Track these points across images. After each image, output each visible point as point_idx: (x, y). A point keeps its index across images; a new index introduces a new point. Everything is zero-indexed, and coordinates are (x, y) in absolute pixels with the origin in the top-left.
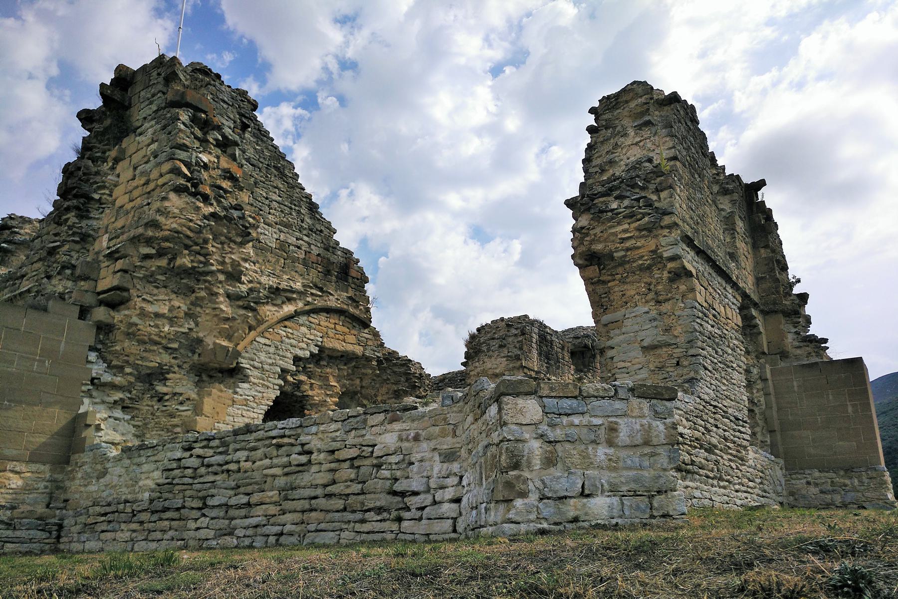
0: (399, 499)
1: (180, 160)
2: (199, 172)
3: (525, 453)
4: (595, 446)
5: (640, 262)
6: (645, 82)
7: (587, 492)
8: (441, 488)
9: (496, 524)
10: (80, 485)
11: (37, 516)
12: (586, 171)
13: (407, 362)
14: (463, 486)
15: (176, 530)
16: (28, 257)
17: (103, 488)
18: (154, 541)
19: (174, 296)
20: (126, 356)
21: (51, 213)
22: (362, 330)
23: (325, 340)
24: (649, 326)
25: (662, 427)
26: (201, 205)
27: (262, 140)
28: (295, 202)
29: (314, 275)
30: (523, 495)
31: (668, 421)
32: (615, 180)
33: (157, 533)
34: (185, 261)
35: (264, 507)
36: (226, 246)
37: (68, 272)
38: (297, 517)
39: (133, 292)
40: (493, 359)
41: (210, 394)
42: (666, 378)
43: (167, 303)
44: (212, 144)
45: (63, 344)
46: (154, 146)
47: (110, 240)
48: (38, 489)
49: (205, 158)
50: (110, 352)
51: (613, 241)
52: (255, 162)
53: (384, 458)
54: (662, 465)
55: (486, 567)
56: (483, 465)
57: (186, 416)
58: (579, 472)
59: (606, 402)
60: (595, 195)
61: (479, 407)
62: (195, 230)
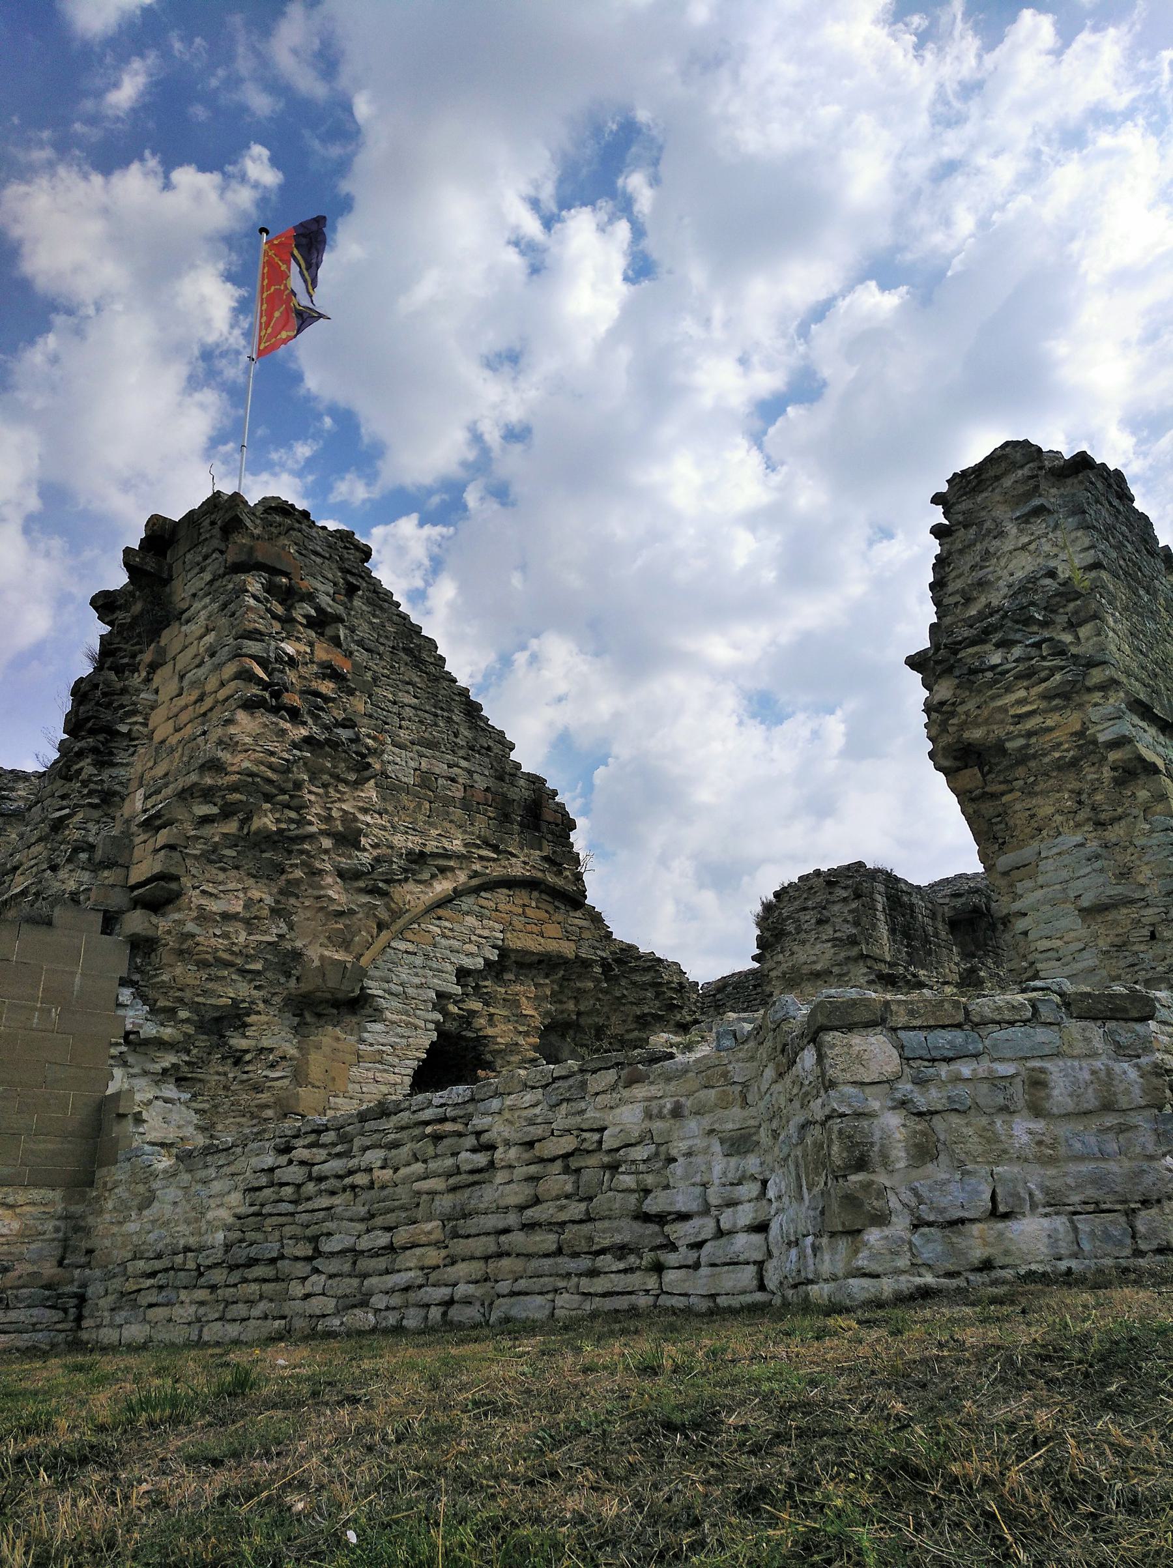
0: (653, 1228)
1: (251, 657)
2: (282, 671)
3: (876, 1138)
4: (1007, 1118)
5: (1057, 755)
6: (1026, 441)
7: (1002, 1208)
8: (728, 1205)
9: (834, 1278)
10: (112, 1223)
11: (44, 1282)
12: (937, 602)
13: (655, 963)
14: (770, 1200)
15: (271, 1300)
16: (21, 836)
17: (149, 1226)
18: (235, 1320)
19: (252, 881)
20: (179, 989)
21: (56, 762)
22: (571, 914)
23: (509, 935)
24: (1089, 869)
25: (1133, 1074)
26: (288, 726)
27: (382, 609)
28: (441, 704)
29: (481, 825)
30: (881, 1219)
31: (1143, 1060)
32: (991, 615)
33: (240, 1305)
34: (267, 821)
35: (418, 1251)
36: (331, 790)
37: (83, 856)
38: (474, 1268)
39: (186, 881)
40: (808, 945)
41: (318, 1047)
42: (1133, 965)
43: (241, 895)
44: (301, 624)
45: (77, 979)
46: (210, 638)
47: (147, 798)
48: (44, 1233)
49: (289, 648)
50: (153, 986)
51: (1002, 722)
52: (372, 645)
53: (621, 1152)
54: (1144, 1148)
55: (806, 1407)
56: (801, 1161)
57: (282, 1088)
58: (984, 1170)
59: (1017, 1032)
60: (960, 643)
61: (783, 1051)
62: (281, 768)
